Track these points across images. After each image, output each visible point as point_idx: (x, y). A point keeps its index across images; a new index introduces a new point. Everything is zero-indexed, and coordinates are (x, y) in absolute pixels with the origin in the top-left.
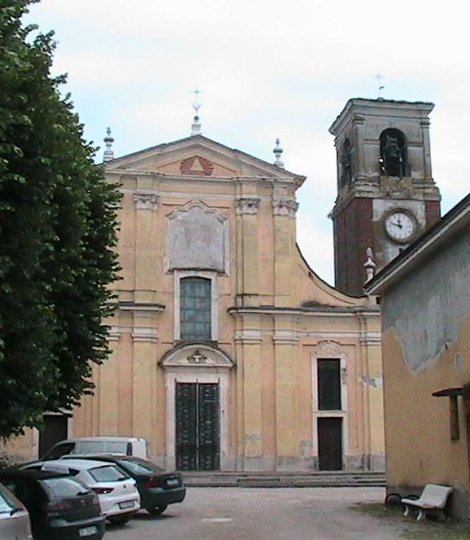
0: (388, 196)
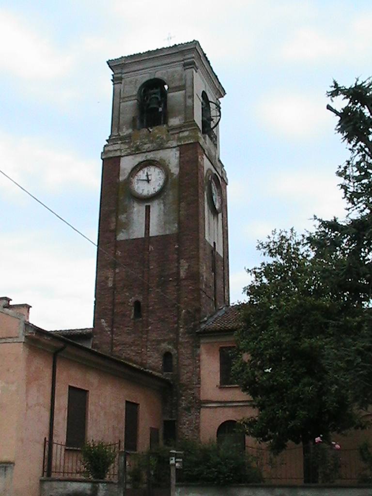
0: (137, 151)
